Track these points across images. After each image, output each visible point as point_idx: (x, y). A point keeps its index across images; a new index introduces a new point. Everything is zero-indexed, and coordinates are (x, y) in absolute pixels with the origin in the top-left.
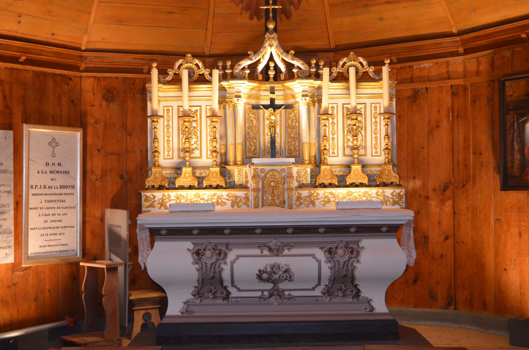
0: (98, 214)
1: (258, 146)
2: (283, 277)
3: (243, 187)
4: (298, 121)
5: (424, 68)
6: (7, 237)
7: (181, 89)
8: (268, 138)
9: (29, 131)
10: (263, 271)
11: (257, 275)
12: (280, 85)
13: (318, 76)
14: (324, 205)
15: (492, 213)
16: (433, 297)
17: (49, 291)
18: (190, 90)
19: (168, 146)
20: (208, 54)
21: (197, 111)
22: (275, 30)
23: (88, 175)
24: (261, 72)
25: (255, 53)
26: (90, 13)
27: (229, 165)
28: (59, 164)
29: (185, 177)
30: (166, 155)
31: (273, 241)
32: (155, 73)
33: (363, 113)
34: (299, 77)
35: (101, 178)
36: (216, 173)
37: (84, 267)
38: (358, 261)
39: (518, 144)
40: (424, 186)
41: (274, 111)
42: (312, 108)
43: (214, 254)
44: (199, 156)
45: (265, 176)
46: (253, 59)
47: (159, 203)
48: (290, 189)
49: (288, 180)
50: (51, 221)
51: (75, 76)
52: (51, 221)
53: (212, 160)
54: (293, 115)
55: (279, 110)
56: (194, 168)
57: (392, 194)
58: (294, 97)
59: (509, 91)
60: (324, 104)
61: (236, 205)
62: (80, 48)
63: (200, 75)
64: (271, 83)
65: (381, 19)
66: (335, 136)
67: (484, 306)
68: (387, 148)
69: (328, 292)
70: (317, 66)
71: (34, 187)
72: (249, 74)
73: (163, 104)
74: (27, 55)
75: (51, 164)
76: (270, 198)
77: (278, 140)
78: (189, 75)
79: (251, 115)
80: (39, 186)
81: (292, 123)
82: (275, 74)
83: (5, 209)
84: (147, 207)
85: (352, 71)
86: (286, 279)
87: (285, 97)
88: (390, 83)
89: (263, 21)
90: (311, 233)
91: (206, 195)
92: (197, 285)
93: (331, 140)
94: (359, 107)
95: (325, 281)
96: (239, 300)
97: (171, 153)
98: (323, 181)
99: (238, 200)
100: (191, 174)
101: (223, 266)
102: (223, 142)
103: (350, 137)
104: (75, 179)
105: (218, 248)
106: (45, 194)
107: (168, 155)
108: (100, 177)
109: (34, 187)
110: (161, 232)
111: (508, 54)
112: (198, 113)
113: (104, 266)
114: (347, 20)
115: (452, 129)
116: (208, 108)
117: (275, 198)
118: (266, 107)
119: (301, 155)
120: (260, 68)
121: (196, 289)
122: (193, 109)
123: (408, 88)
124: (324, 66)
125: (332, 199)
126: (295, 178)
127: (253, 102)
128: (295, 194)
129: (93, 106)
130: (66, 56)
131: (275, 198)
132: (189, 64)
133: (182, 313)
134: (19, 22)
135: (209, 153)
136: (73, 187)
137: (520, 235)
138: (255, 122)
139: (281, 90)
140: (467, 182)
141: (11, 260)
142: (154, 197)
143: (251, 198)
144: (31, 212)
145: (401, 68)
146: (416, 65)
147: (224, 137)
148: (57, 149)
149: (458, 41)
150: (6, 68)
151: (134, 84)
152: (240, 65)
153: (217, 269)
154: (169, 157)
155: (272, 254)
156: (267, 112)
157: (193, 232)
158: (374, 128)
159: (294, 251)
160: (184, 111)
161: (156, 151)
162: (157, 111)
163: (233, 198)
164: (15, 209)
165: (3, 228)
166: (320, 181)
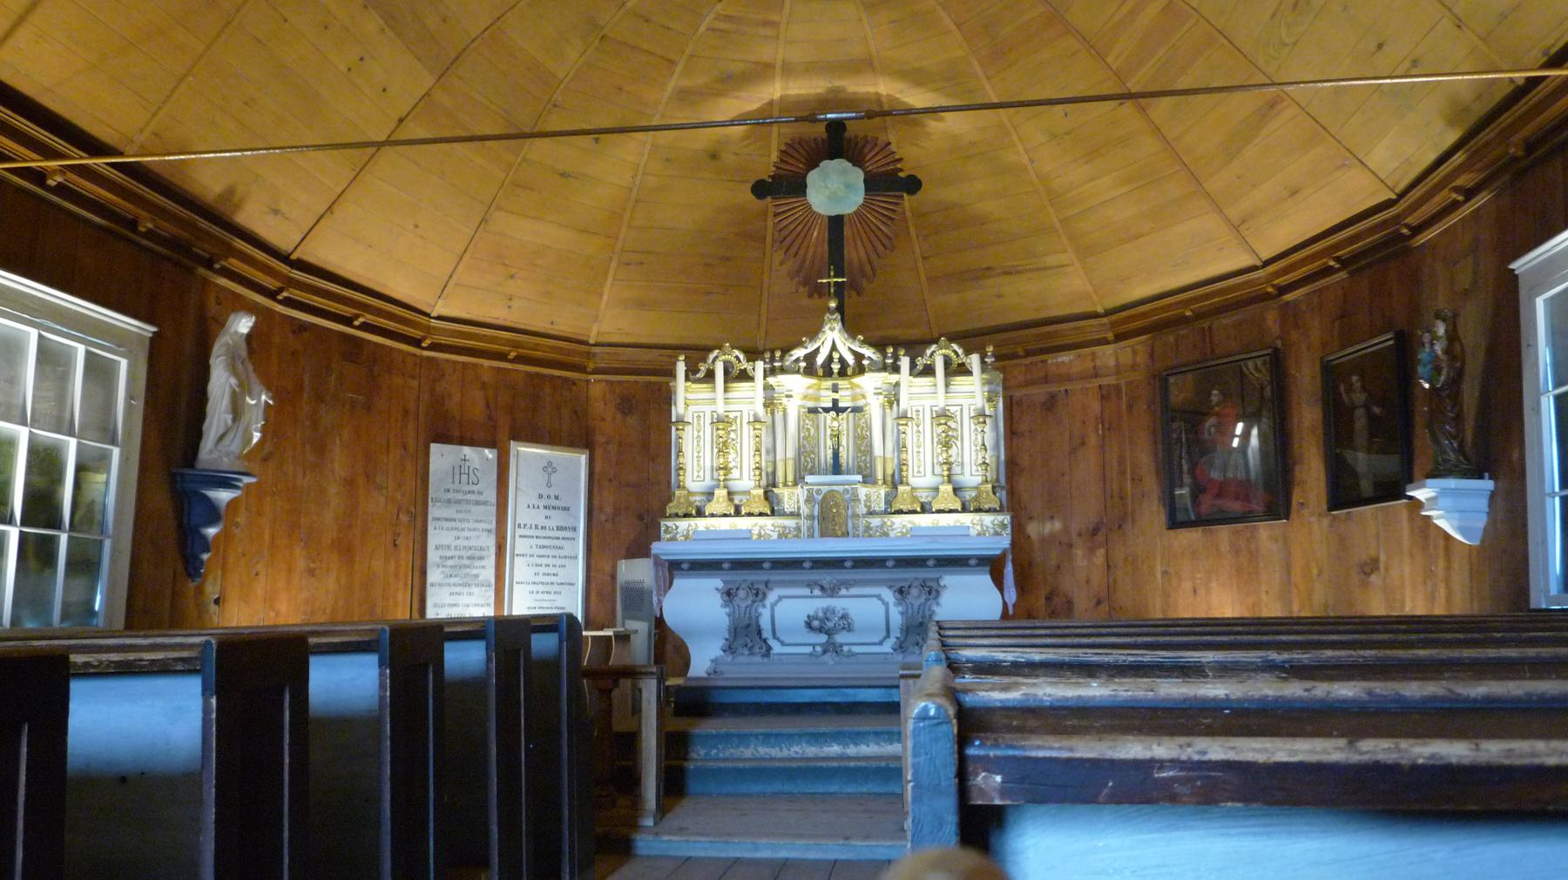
0: (608, 568)
1: (817, 463)
2: (839, 625)
3: (795, 515)
4: (870, 429)
5: (1063, 362)
6: (486, 591)
8: (830, 453)
9: (518, 451)
10: (813, 616)
11: (806, 622)
12: (846, 382)
13: (896, 369)
18: (726, 390)
21: (736, 417)
23: (595, 513)
24: (823, 366)
25: (811, 341)
26: (601, 295)
29: (718, 502)
30: (695, 476)
31: (827, 577)
32: (681, 368)
35: (613, 518)
37: (587, 637)
38: (938, 604)
39: (1187, 463)
40: (1066, 530)
41: (838, 415)
42: (888, 411)
44: (739, 477)
47: (683, 536)
48: (855, 516)
49: (853, 504)
50: (544, 574)
51: (579, 380)
52: (544, 574)
54: (863, 420)
55: (845, 414)
57: (992, 522)
58: (864, 397)
59: (1173, 390)
60: (904, 404)
63: (740, 370)
64: (835, 379)
65: (999, 296)
68: (984, 463)
71: (522, 526)
72: (805, 368)
74: (520, 350)
75: (545, 496)
79: (807, 421)
81: (862, 432)
82: (840, 369)
83: (484, 553)
86: (843, 628)
87: (854, 398)
91: (742, 523)
94: (952, 409)
95: (896, 633)
96: (783, 657)
97: (701, 474)
100: (726, 499)
101: (761, 610)
102: (771, 458)
104: (577, 518)
105: (755, 587)
106: (537, 537)
108: (611, 517)
109: (522, 526)
110: (683, 566)
111: (1171, 339)
114: (953, 299)
115: (1102, 448)
118: (827, 410)
119: (873, 475)
120: (820, 359)
126: (863, 502)
127: (811, 404)
128: (862, 522)
129: (603, 419)
130: (569, 353)
131: (837, 528)
132: (727, 356)
133: (709, 674)
134: (510, 307)
136: (575, 529)
137: (1195, 591)
138: (812, 431)
139: (847, 388)
142: (677, 527)
143: (804, 529)
145: (1031, 363)
146: (1052, 359)
148: (554, 476)
149: (1106, 324)
151: (659, 390)
153: (753, 615)
154: (699, 479)
155: (824, 595)
159: (854, 591)
161: (681, 468)
163: (780, 529)
165: (480, 578)
166: (896, 506)
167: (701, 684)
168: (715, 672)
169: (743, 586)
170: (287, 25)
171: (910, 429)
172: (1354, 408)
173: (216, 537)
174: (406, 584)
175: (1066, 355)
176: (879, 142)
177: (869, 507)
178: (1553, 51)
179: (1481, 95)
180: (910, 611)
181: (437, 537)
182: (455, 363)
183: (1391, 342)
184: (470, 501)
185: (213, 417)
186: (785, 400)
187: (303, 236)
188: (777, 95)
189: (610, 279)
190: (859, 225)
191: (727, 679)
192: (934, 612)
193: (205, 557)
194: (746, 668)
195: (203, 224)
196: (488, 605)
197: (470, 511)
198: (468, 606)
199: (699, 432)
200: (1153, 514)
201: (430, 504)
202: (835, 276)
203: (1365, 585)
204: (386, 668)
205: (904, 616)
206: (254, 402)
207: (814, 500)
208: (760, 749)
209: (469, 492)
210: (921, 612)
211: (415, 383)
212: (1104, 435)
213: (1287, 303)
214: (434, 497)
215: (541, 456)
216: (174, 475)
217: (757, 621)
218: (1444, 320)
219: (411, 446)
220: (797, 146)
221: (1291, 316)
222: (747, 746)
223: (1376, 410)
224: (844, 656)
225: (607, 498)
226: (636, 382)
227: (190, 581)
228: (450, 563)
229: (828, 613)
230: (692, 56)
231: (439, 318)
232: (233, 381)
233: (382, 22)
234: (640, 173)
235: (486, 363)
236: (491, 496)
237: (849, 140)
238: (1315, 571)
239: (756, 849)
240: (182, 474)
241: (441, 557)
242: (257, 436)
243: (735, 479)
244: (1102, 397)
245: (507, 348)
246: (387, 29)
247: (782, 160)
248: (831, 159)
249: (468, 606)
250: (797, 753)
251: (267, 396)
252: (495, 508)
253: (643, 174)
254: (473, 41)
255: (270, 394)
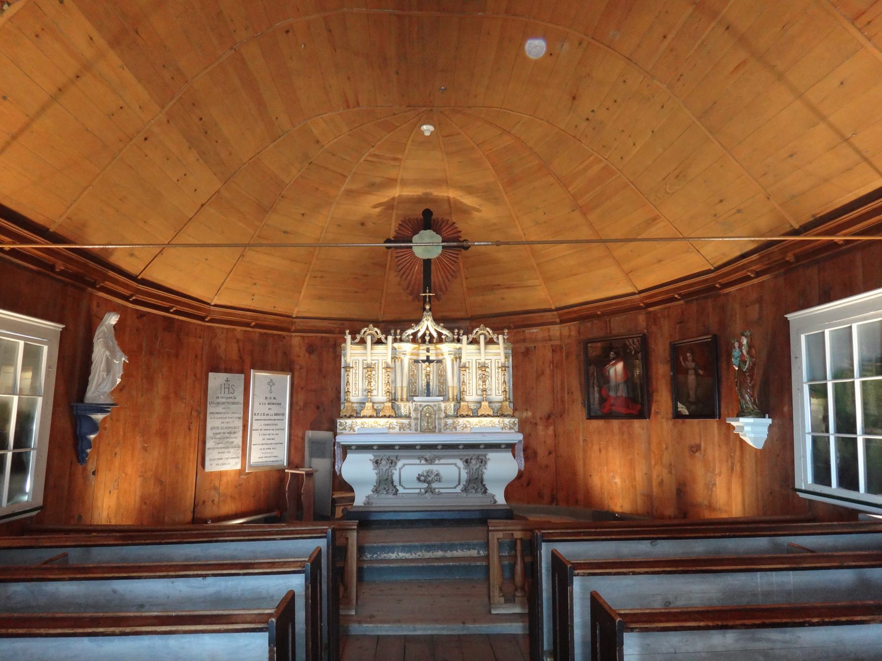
0: (300, 434)
3: (408, 417)
4: (445, 371)
6: (237, 450)
7: (366, 348)
8: (424, 383)
9: (255, 375)
11: (417, 478)
13: (459, 341)
14: (463, 430)
15: (581, 435)
16: (540, 496)
17: (264, 489)
18: (372, 349)
19: (355, 388)
20: (381, 320)
22: (430, 309)
24: (420, 337)
26: (300, 292)
27: (397, 401)
28: (274, 398)
29: (367, 409)
30: (354, 393)
31: (428, 454)
33: (489, 366)
34: (446, 341)
36: (389, 407)
37: (288, 473)
38: (486, 468)
40: (534, 417)
41: (429, 364)
42: (455, 362)
43: (388, 463)
45: (423, 409)
46: (415, 329)
47: (349, 427)
48: (440, 418)
52: (268, 439)
53: (386, 398)
54: (442, 367)
55: (433, 364)
56: (374, 403)
58: (442, 354)
60: (463, 360)
61: (402, 430)
62: (292, 316)
65: (503, 299)
66: (471, 382)
67: (577, 502)
68: (505, 391)
69: (465, 490)
70: (459, 334)
71: (257, 414)
72: (412, 339)
73: (353, 358)
74: (257, 321)
75: (268, 398)
76: (426, 424)
77: (431, 384)
78: (372, 340)
79: (413, 367)
80: (260, 414)
84: (341, 430)
85: (482, 338)
87: (437, 355)
88: (505, 346)
89: (422, 303)
90: (390, 449)
92: (375, 485)
93: (468, 384)
94: (487, 361)
95: (463, 482)
97: (357, 392)
98: (463, 413)
99: (404, 426)
100: (371, 407)
101: (393, 471)
102: (394, 385)
103: (480, 382)
104: (285, 409)
107: (355, 394)
109: (257, 414)
112: (377, 365)
113: (304, 473)
115: (552, 376)
116: (384, 361)
117: (429, 424)
118: (424, 361)
120: (420, 334)
121: (375, 488)
122: (373, 362)
123: (522, 347)
124: (463, 334)
125: (468, 426)
127: (415, 358)
129: (299, 356)
131: (429, 424)
133: (365, 504)
134: (253, 299)
135: (384, 392)
136: (284, 414)
138: (415, 372)
140: (563, 413)
141: (239, 467)
142: (346, 423)
143: (413, 424)
144: (254, 432)
147: (395, 381)
150: (242, 330)
152: (406, 333)
153: (390, 474)
156: (425, 365)
157: (374, 447)
158: (497, 376)
159: (442, 461)
160: (367, 364)
162: (349, 364)
164: (243, 430)
165: (234, 443)
167: (360, 509)
168: (368, 503)
169: (384, 458)
170: (147, 158)
171: (466, 373)
172: (688, 369)
173: (95, 439)
174: (195, 450)
175: (535, 329)
176: (449, 222)
177: (445, 413)
178: (818, 216)
179: (772, 230)
180: (471, 472)
181: (212, 423)
182: (223, 328)
183: (710, 340)
184: (229, 402)
185: (95, 372)
186: (402, 356)
187: (145, 266)
188: (397, 195)
189: (306, 283)
190: (439, 264)
191: (376, 507)
192: (483, 472)
193: (89, 451)
194: (385, 501)
195: (92, 264)
196: (238, 458)
197: (229, 408)
198: (228, 459)
199: (356, 370)
200: (578, 411)
201: (208, 405)
202: (429, 292)
203: (692, 457)
204: (274, 647)
205: (468, 474)
206: (118, 362)
207: (418, 410)
208: (400, 554)
209: (229, 398)
210: (477, 473)
211: (201, 340)
212: (553, 370)
213: (650, 312)
214: (210, 401)
215: (266, 377)
216: (73, 406)
217: (392, 477)
218: (746, 337)
219: (198, 375)
220: (408, 222)
221: (653, 319)
222: (393, 553)
223: (701, 372)
224: (435, 494)
225: (301, 397)
226: (316, 337)
227: (79, 464)
228: (218, 436)
229: (429, 473)
230: (355, 173)
231: (215, 306)
232: (107, 353)
233: (198, 156)
234: (324, 231)
235: (239, 328)
236: (240, 398)
237: (434, 220)
238: (664, 446)
239: (415, 630)
240: (77, 406)
241: (213, 434)
242: (119, 380)
243: (375, 396)
244: (553, 351)
245: (251, 321)
246: (200, 159)
247: (399, 229)
248: (425, 230)
249: (228, 459)
250: (419, 556)
251: (125, 358)
252: (242, 406)
253: (326, 232)
254: (244, 164)
255: (127, 357)
